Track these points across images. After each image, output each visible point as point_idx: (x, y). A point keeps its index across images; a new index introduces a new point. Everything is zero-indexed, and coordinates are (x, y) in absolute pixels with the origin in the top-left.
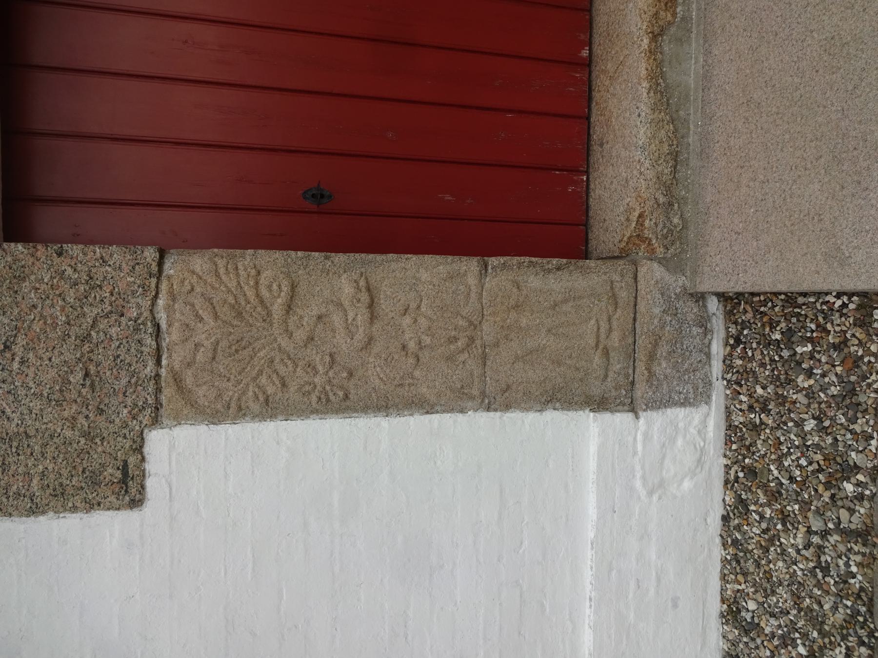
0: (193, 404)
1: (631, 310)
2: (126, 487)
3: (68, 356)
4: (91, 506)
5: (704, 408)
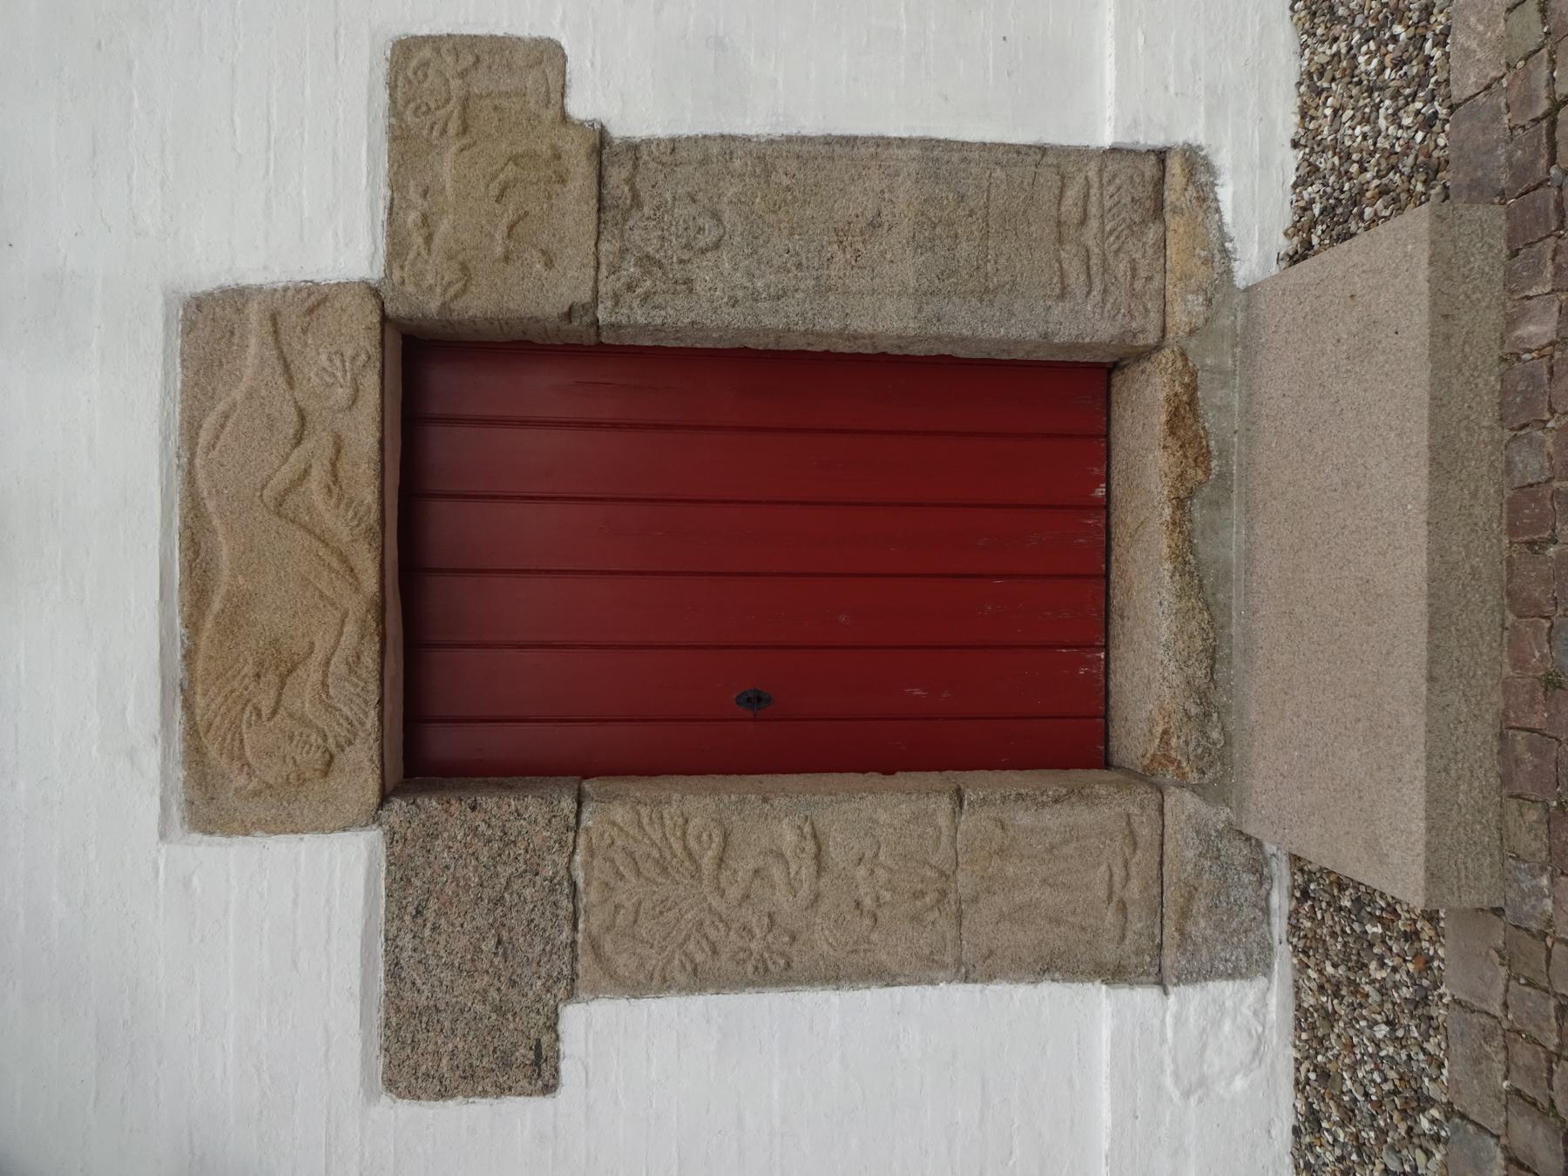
2: (539, 1070)
3: (480, 922)
4: (502, 1090)
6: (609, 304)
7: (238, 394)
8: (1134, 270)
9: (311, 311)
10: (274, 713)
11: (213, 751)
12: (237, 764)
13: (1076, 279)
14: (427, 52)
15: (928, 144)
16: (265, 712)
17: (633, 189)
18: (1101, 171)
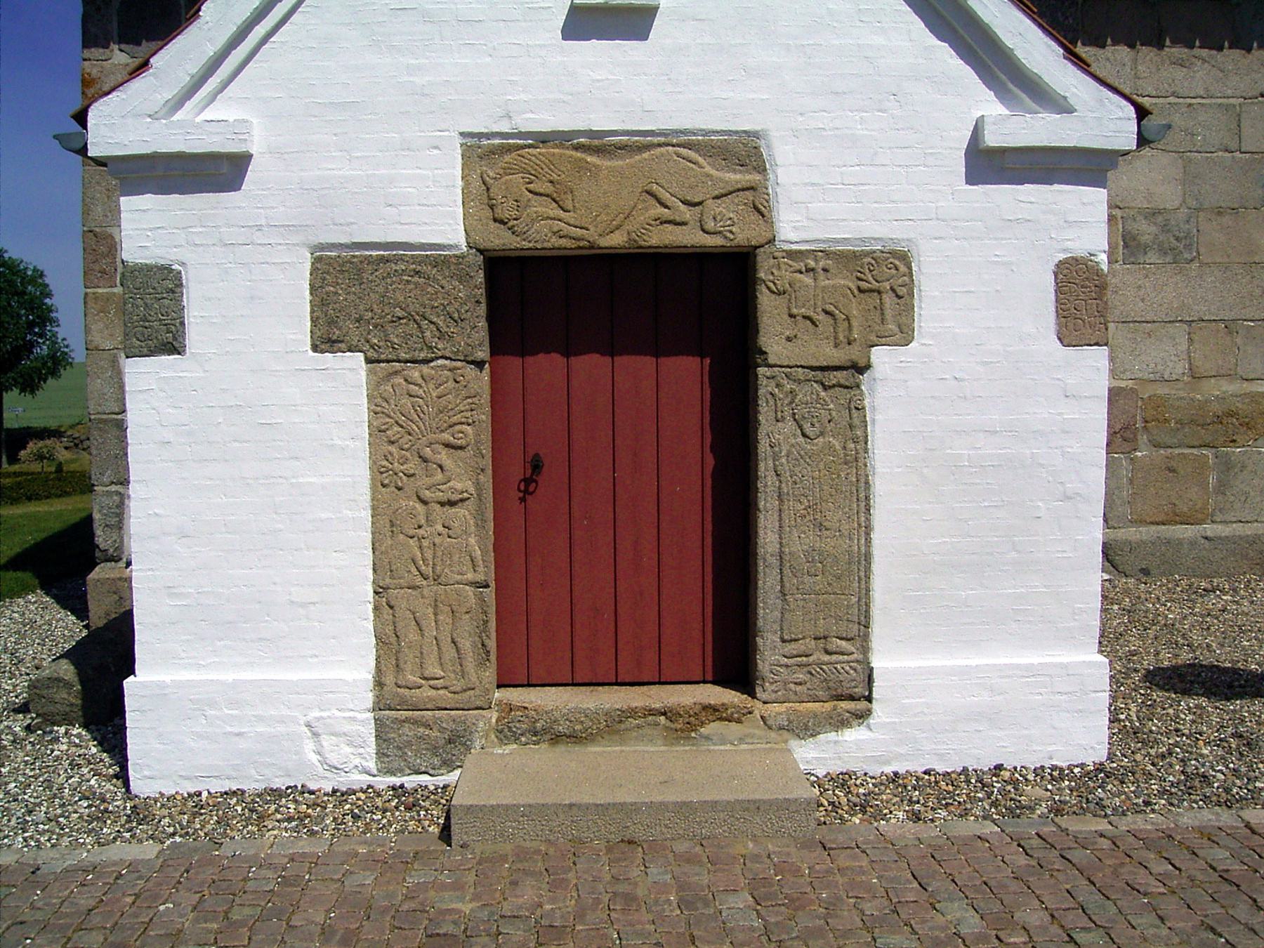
0: (378, 384)
1: (453, 706)
2: (325, 342)
3: (411, 308)
4: (314, 321)
5: (372, 765)
6: (768, 374)
7: (708, 169)
8: (800, 684)
9: (756, 208)
10: (530, 191)
11: (507, 158)
12: (501, 172)
13: (791, 648)
14: (903, 268)
15: (868, 557)
16: (531, 186)
17: (834, 386)
18: (858, 661)
